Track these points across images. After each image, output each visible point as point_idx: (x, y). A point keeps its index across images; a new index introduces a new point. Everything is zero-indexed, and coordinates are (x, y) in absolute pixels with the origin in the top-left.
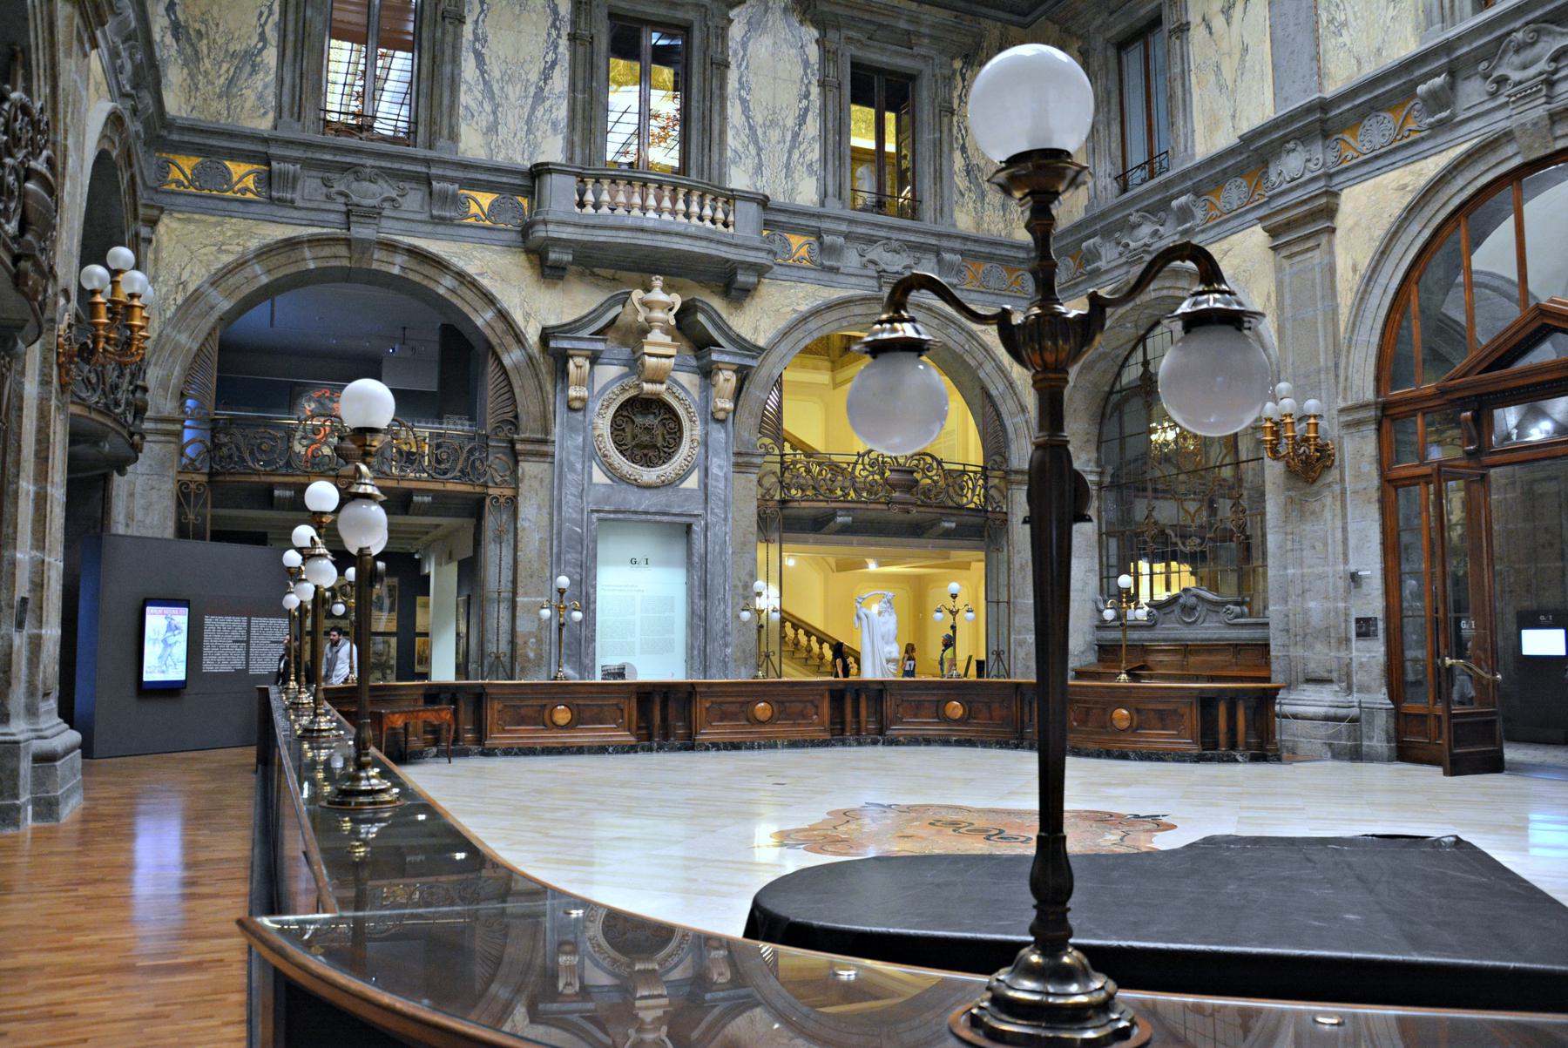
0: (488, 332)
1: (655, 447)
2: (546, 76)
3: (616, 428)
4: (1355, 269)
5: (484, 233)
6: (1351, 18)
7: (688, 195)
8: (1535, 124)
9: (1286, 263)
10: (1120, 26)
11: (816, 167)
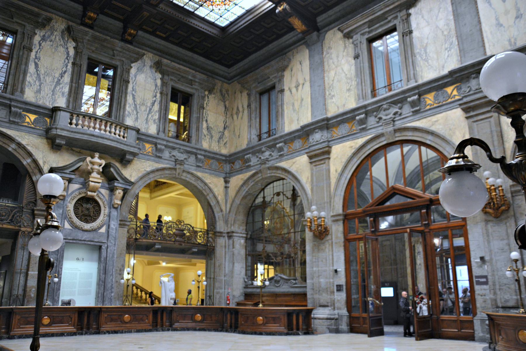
0: (28, 167)
1: (90, 216)
2: (62, 76)
3: (76, 208)
4: (336, 171)
5: (30, 129)
6: (336, 94)
7: (111, 125)
8: (390, 132)
9: (314, 168)
10: (261, 88)
11: (157, 121)
